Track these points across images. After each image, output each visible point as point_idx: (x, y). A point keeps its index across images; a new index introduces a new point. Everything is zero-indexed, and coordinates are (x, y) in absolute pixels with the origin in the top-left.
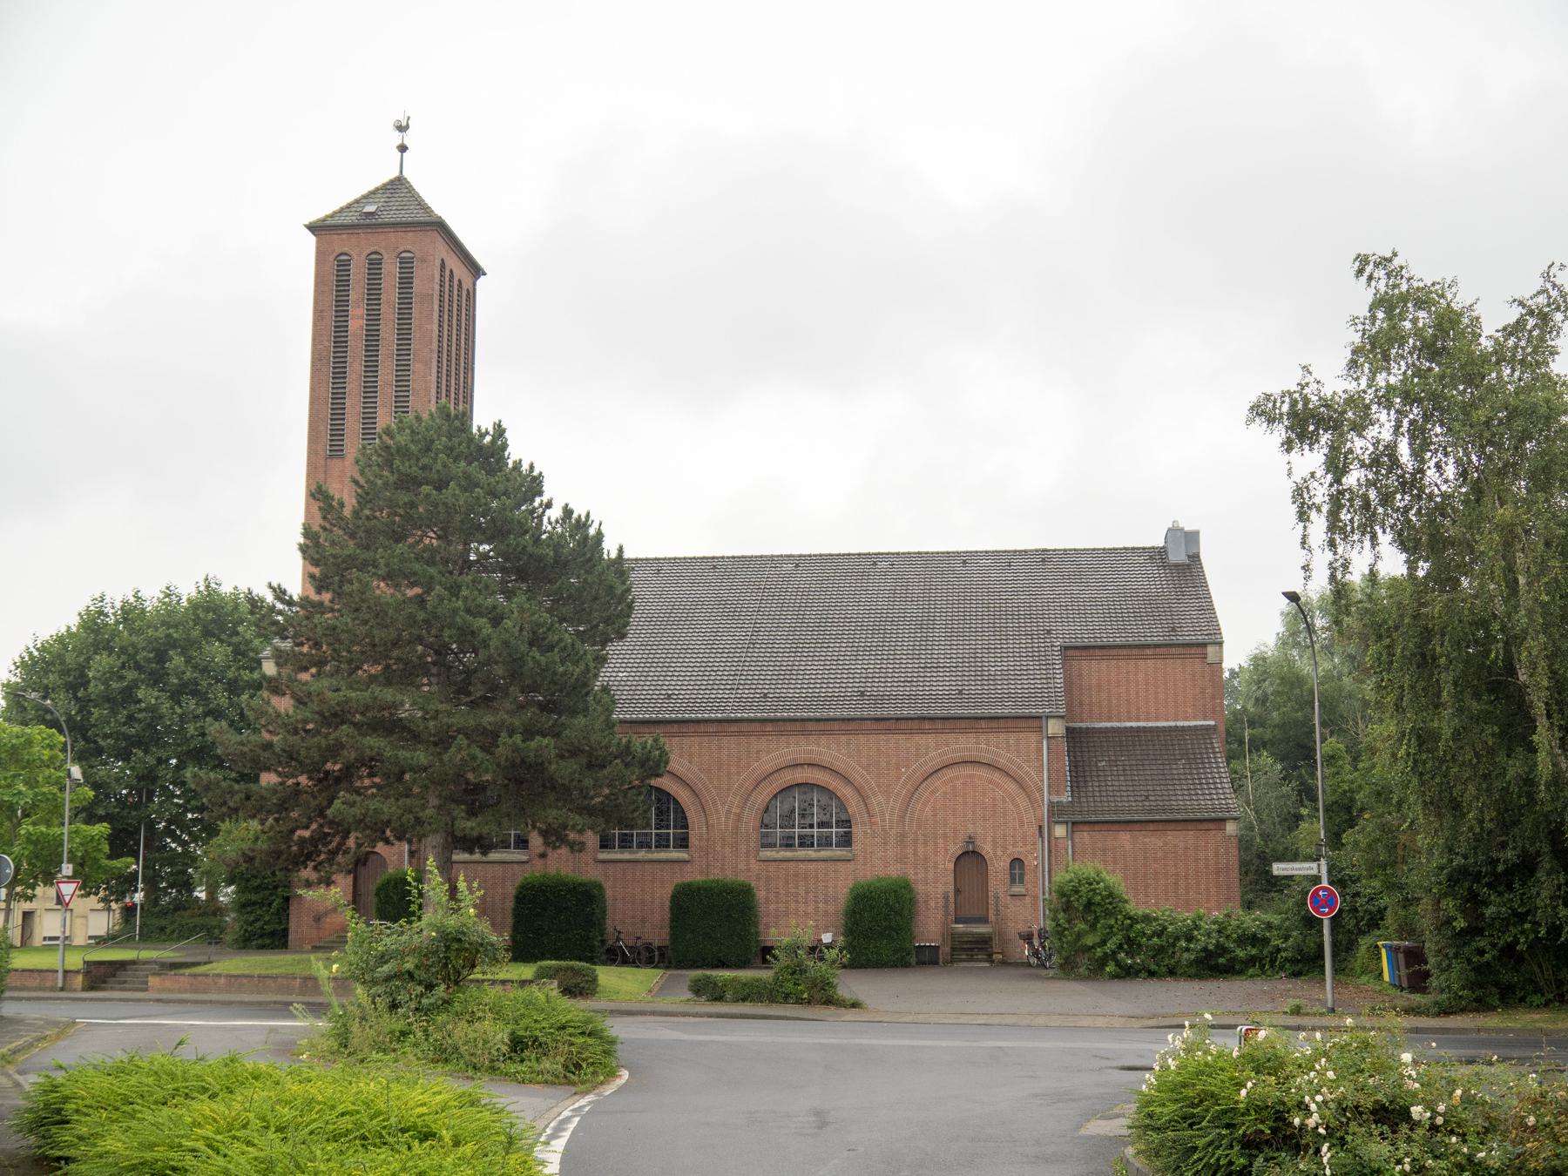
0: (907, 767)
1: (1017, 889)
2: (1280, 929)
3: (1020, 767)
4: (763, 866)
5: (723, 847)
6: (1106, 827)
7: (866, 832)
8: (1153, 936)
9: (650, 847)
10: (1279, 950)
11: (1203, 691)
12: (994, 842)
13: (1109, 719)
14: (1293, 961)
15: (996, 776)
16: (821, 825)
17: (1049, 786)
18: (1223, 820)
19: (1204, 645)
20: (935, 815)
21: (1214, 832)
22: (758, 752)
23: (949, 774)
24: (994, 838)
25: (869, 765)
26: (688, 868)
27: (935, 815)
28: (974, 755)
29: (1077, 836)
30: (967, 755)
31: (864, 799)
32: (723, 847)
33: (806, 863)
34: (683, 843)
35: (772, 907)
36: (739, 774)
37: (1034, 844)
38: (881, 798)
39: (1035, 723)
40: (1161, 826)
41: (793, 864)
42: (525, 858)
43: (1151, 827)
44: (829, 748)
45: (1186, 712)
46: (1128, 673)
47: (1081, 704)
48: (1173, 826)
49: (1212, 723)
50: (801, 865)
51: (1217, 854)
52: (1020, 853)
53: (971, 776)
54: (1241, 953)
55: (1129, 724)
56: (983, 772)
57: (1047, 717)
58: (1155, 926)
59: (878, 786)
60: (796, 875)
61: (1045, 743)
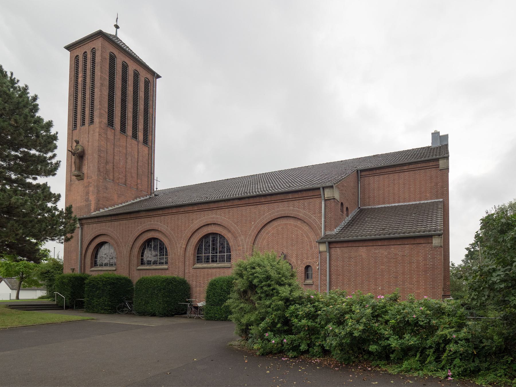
0: (255, 221)
1: (309, 282)
2: (454, 315)
3: (310, 218)
4: (195, 270)
5: (179, 263)
6: (350, 244)
7: (237, 254)
8: (302, 318)
9: (157, 264)
10: (447, 341)
11: (436, 184)
12: (297, 256)
13: (384, 203)
14: (464, 357)
15: (299, 223)
16: (220, 252)
17: (325, 226)
18: (431, 236)
19: (437, 160)
20: (268, 245)
21: (424, 245)
22: (192, 220)
23: (275, 223)
24: (297, 255)
25: (238, 222)
26: (167, 272)
27: (268, 245)
28: (287, 213)
29: (333, 250)
30: (283, 214)
31: (236, 238)
32: (179, 263)
33: (212, 269)
34: (166, 263)
35: (198, 289)
36: (185, 230)
37: (318, 257)
38: (243, 237)
39: (316, 193)
40: (386, 243)
41: (207, 270)
42: (114, 269)
43: (379, 243)
44: (221, 216)
45: (426, 196)
46: (394, 180)
47: (369, 197)
48: (393, 242)
49: (442, 200)
50: (210, 270)
51: (425, 259)
52: (310, 262)
53: (286, 224)
54: (394, 343)
55: (393, 205)
56: (291, 222)
57: (324, 188)
58: (309, 308)
59: (241, 232)
60: (208, 275)
61: (323, 202)
